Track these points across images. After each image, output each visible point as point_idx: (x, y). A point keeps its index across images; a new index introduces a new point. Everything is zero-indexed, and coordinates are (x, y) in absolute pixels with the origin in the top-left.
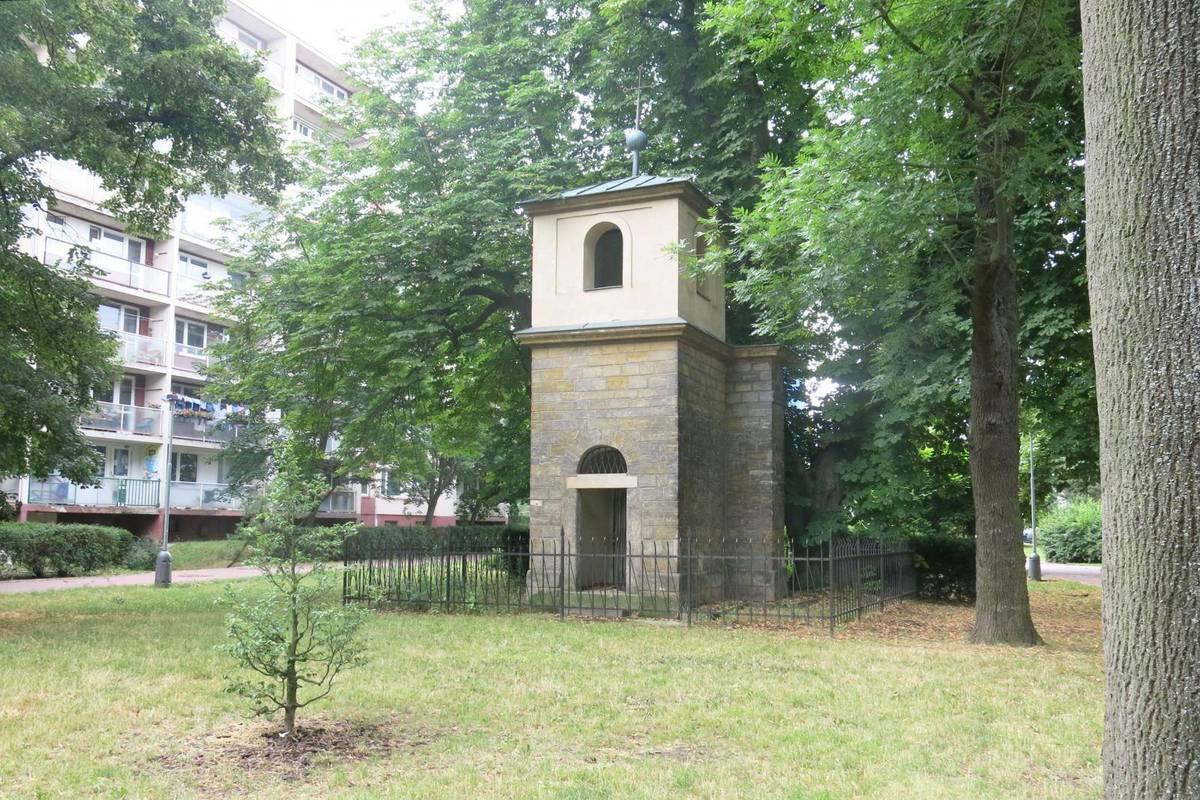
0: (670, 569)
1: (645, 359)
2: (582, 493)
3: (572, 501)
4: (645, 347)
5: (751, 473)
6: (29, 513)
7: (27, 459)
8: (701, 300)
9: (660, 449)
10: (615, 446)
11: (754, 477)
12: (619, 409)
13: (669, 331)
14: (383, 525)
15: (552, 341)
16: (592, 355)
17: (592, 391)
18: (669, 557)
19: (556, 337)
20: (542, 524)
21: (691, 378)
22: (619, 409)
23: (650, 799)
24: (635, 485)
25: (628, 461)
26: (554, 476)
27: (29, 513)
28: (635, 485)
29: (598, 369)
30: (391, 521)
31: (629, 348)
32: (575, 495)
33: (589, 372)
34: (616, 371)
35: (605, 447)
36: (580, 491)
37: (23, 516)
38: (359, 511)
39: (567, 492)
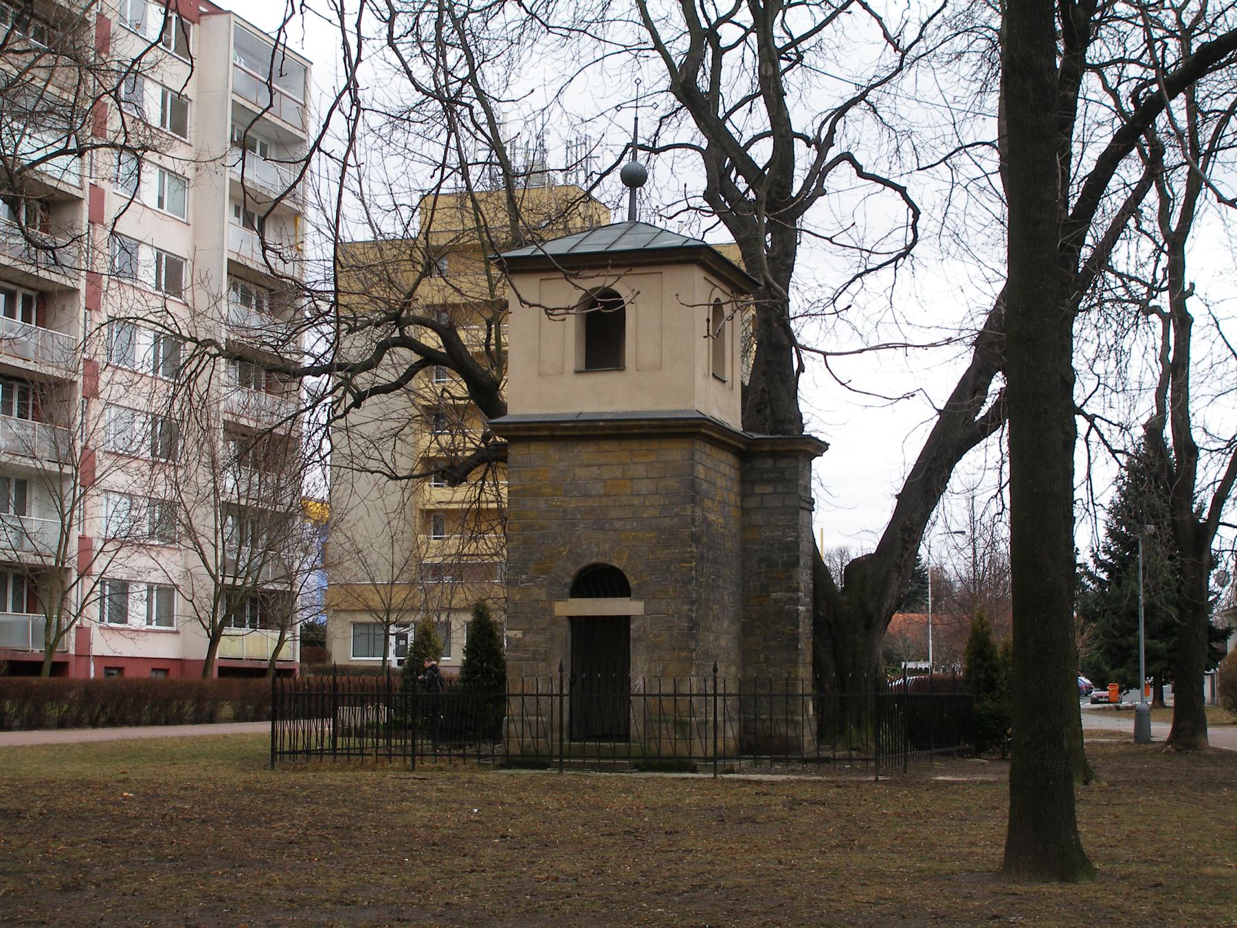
0: (557, 710)
1: (653, 458)
2: (576, 622)
3: (564, 632)
4: (654, 445)
5: (773, 595)
6: (220, 668)
7: (786, 607)
8: (717, 383)
9: (672, 568)
10: (615, 564)
11: (776, 601)
12: (620, 519)
13: (684, 426)
14: (102, 675)
15: (534, 433)
16: (587, 452)
17: (588, 496)
18: (706, 695)
19: (540, 429)
20: (522, 659)
21: (706, 481)
22: (620, 519)
23: (992, 927)
24: (641, 612)
25: (633, 583)
26: (537, 601)
27: (220, 668)
28: (641, 612)
29: (595, 470)
30: (114, 666)
31: (634, 445)
32: (566, 624)
33: (581, 472)
34: (618, 473)
35: (606, 565)
36: (571, 619)
37: (47, 669)
38: (72, 651)
39: (555, 621)
